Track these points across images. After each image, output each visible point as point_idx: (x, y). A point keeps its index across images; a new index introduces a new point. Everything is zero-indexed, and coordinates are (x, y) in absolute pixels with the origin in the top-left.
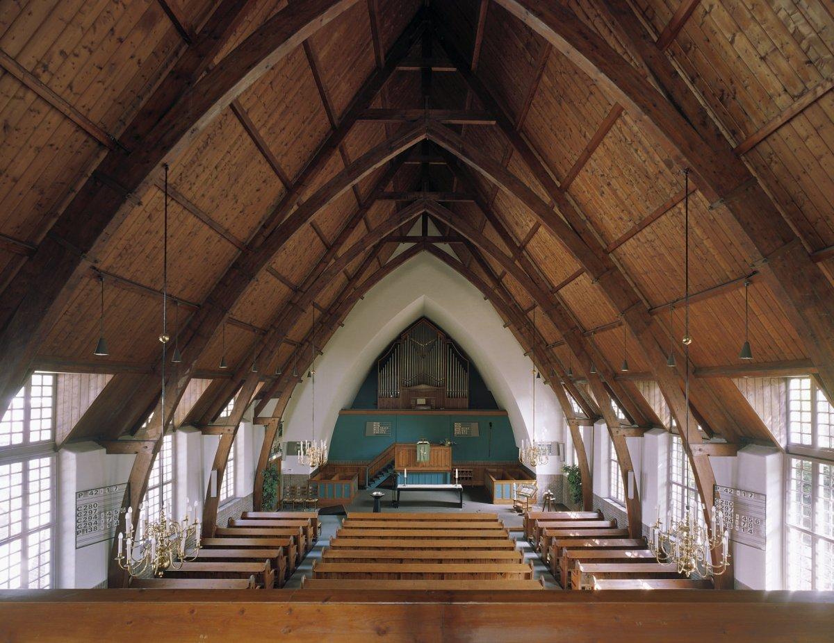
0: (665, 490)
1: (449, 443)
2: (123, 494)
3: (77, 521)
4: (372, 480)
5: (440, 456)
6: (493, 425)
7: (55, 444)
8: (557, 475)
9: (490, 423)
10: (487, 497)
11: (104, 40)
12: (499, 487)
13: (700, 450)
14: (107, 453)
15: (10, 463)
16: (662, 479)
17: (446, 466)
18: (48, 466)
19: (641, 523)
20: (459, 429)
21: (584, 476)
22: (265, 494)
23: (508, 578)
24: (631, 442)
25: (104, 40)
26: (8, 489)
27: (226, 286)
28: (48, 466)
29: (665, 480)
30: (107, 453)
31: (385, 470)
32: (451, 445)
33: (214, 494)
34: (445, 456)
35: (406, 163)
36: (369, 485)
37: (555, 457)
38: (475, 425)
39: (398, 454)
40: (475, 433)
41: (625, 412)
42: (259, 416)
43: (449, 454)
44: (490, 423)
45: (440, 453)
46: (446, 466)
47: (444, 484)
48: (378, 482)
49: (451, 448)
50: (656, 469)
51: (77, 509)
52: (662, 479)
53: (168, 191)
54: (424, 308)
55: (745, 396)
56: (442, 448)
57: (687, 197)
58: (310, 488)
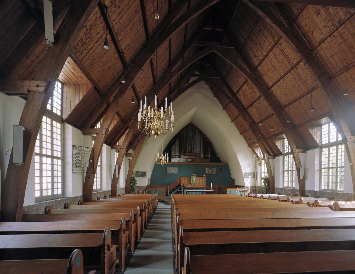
0: (318, 173)
2: (90, 153)
3: (72, 160)
7: (62, 119)
8: (254, 186)
9: (221, 169)
10: (225, 193)
12: (229, 190)
13: (350, 138)
15: (36, 139)
16: (317, 168)
18: (47, 159)
19: (305, 190)
20: (208, 171)
21: (271, 180)
22: (131, 189)
24: (302, 156)
26: (48, 131)
27: (141, 55)
28: (47, 159)
29: (318, 168)
32: (205, 176)
33: (117, 176)
34: (203, 181)
35: (204, 28)
37: (253, 178)
38: (214, 169)
39: (183, 180)
40: (215, 173)
41: (269, 176)
42: (128, 152)
44: (221, 169)
46: (203, 185)
50: (315, 163)
51: (73, 154)
52: (317, 168)
53: (41, 155)
54: (193, 117)
56: (202, 178)
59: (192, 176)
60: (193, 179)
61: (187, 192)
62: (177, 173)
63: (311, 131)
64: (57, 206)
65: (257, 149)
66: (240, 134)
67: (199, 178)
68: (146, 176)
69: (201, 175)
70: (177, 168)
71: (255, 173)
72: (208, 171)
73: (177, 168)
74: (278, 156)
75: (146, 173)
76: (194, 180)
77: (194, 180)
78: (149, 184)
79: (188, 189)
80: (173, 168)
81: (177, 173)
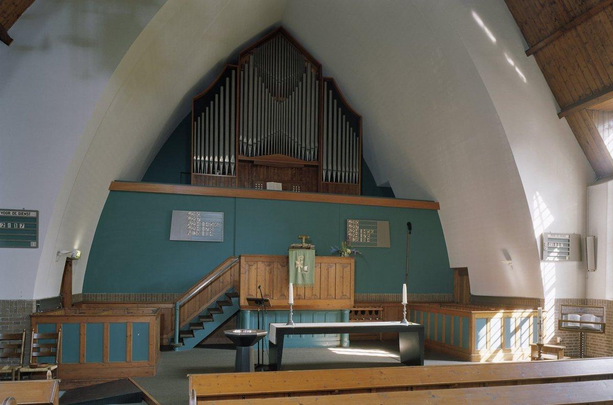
1: (349, 251)
4: (188, 332)
5: (332, 276)
6: (412, 226)
9: (409, 225)
11: (544, 211)
14: (439, 209)
17: (343, 297)
23: (507, 262)
25: (544, 211)
30: (439, 209)
31: (218, 308)
32: (351, 255)
36: (181, 340)
40: (384, 241)
43: (349, 271)
44: (409, 225)
45: (332, 270)
47: (341, 322)
48: (200, 335)
49: (353, 261)
55: (596, 126)
56: (336, 259)
57: (542, 223)
58: (35, 336)
59: (292, 254)
60: (299, 265)
61: (281, 333)
62: (220, 238)
63: (600, 129)
64: (104, 295)
65: (606, 126)
66: (528, 53)
67: (326, 260)
68: (35, 238)
69: (334, 250)
70: (218, 217)
71: (589, 240)
72: (354, 229)
73: (218, 217)
74: (603, 182)
75: (35, 220)
76: (302, 270)
77: (302, 270)
78: (77, 288)
79: (283, 311)
80: (199, 214)
81: (220, 238)
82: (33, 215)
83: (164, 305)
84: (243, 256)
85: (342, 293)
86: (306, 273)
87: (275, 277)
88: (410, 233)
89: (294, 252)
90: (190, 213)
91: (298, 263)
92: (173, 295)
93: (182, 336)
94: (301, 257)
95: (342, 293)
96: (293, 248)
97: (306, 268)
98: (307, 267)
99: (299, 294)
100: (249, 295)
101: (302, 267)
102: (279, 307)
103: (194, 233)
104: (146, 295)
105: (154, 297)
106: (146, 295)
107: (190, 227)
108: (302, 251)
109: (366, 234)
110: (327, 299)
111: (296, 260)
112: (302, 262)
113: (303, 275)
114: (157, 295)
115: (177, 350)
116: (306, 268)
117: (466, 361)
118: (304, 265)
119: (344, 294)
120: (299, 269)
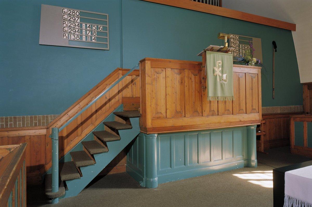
9: (274, 43)
14: (295, 30)
17: (253, 110)
30: (295, 30)
36: (63, 184)
44: (274, 43)
60: (218, 71)
82: (142, 184)
83: (33, 131)
84: (149, 60)
85: (252, 106)
86: (225, 83)
87: (186, 89)
88: (276, 51)
89: (212, 55)
90: (65, 10)
91: (216, 69)
92: (47, 117)
93: (63, 178)
94: (219, 63)
95: (252, 106)
96: (212, 50)
97: (225, 76)
98: (226, 75)
99: (212, 110)
100: (157, 113)
101: (220, 75)
102: (187, 126)
103: (73, 37)
104: (6, 119)
105: (11, 121)
106: (6, 119)
107: (66, 29)
108: (220, 55)
109: (244, 50)
110: (239, 113)
111: (215, 65)
112: (220, 69)
113: (222, 85)
114: (23, 118)
115: (57, 201)
116: (225, 76)
117: (37, 124)
118: (222, 72)
119: (254, 108)
120: (218, 77)
